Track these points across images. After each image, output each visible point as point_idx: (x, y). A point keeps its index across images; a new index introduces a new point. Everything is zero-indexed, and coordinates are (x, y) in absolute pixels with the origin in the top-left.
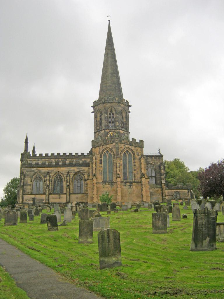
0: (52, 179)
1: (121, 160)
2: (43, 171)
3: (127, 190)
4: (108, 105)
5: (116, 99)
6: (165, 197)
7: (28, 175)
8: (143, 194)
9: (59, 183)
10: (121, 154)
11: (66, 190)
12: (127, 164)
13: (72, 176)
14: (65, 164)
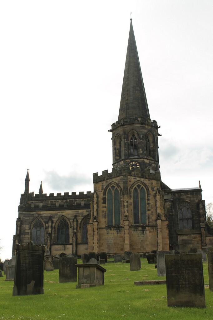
0: (55, 225)
1: (131, 197)
2: (44, 215)
3: (139, 237)
4: (128, 128)
5: (139, 119)
6: (206, 246)
7: (26, 222)
8: (159, 241)
9: (65, 230)
10: (131, 190)
11: (73, 240)
12: (139, 203)
13: (80, 221)
14: (80, 205)
